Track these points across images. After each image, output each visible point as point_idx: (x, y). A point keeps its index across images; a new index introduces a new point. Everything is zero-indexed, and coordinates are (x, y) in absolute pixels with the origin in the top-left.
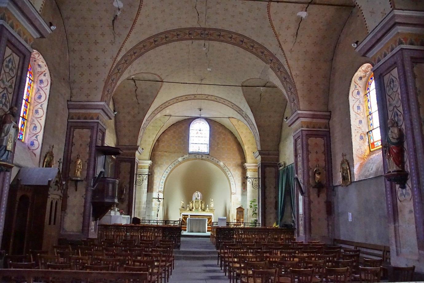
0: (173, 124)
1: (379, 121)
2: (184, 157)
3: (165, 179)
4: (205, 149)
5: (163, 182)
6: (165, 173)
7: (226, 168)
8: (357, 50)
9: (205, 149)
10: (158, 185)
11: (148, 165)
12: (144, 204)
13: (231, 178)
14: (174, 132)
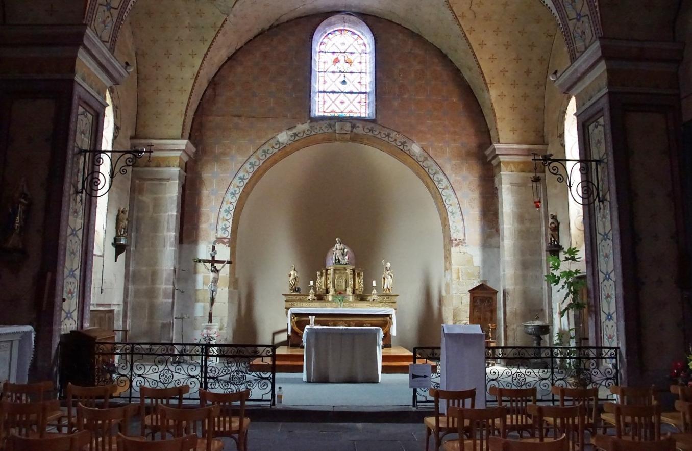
0: (259, 34)
2: (294, 131)
3: (234, 200)
4: (360, 107)
5: (228, 211)
6: (237, 181)
7: (429, 162)
8: (556, 84)
9: (360, 107)
10: (213, 220)
11: (178, 154)
12: (168, 280)
13: (447, 193)
14: (265, 56)
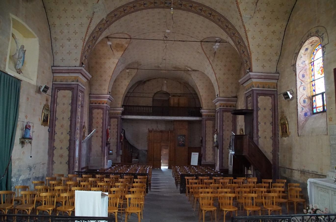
1: (325, 82)
